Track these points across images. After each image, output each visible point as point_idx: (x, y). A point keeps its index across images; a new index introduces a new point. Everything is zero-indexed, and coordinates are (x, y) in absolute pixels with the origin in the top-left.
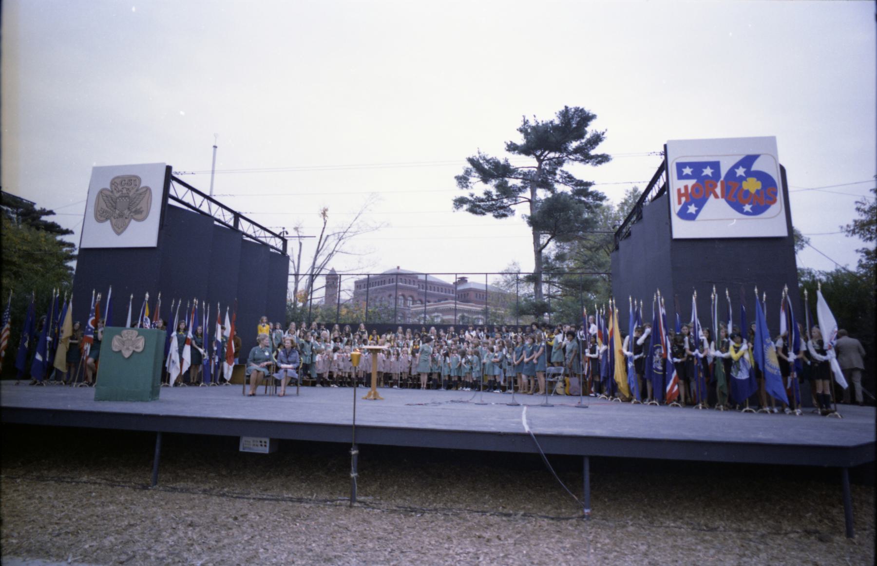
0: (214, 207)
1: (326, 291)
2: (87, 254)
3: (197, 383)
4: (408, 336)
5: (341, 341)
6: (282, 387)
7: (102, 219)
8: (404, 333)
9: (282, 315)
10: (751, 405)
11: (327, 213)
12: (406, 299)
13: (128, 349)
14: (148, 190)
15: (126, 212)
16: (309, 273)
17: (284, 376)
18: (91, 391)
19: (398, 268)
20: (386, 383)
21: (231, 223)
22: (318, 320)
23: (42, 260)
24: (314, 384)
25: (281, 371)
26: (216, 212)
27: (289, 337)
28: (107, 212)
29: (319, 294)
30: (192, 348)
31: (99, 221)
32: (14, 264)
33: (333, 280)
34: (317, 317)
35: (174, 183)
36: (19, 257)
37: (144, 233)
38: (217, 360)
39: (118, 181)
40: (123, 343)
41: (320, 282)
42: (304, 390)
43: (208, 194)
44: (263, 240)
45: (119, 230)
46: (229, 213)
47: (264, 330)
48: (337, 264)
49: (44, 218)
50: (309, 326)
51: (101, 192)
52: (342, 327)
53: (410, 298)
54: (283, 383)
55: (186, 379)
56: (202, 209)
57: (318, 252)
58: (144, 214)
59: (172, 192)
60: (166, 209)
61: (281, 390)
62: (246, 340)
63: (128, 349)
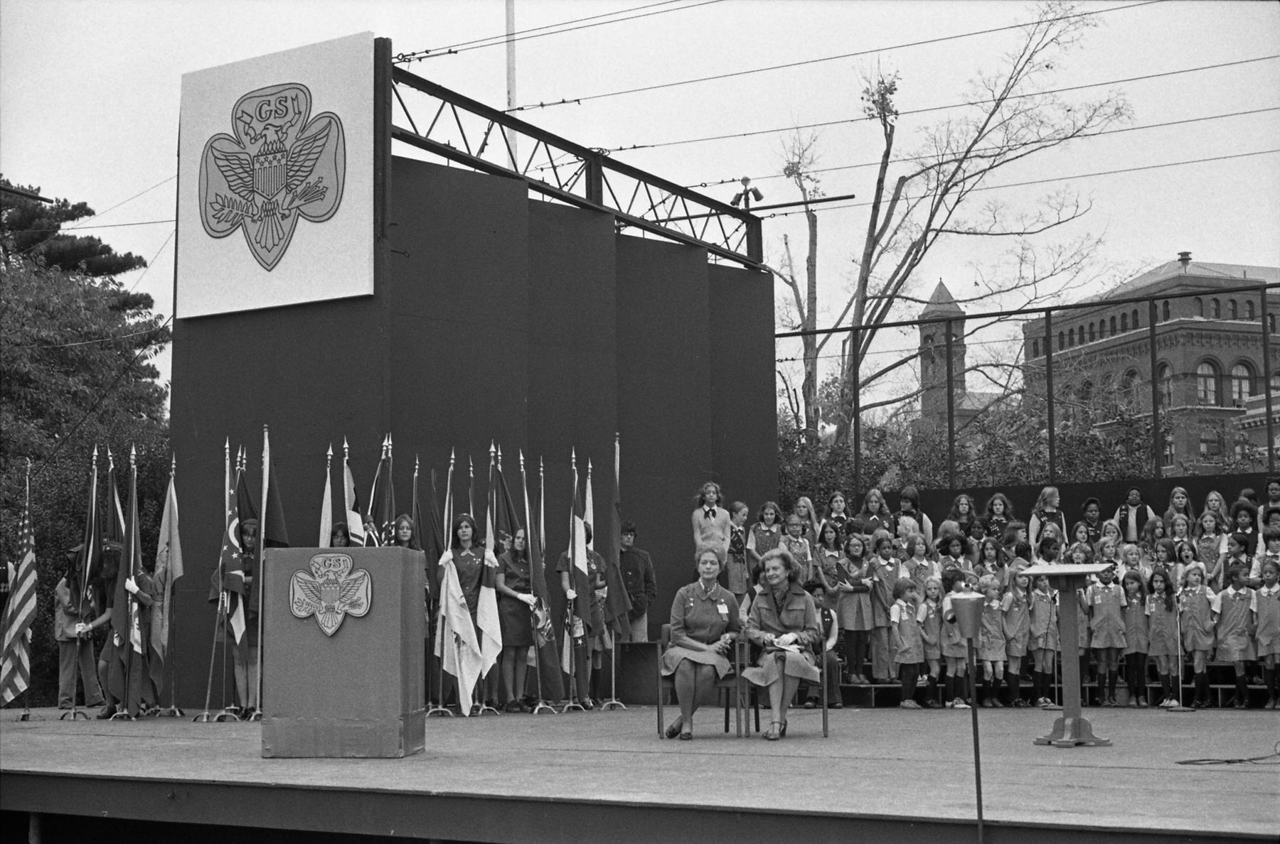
0: (525, 143)
1: (924, 370)
2: (195, 335)
3: (527, 705)
4: (1208, 521)
5: (966, 551)
6: (776, 713)
7: (224, 226)
8: (1196, 506)
9: (768, 471)
10: (546, 699)
11: (895, 100)
12: (1222, 378)
13: (330, 609)
14: (332, 120)
15: (282, 198)
16: (848, 322)
17: (775, 676)
18: (252, 732)
19: (1185, 258)
20: (1136, 691)
21: (580, 190)
22: (889, 479)
23: (82, 364)
24: (888, 699)
25: (768, 659)
26: (531, 160)
27: (788, 549)
28: (232, 203)
29: (893, 384)
30: (501, 596)
31: (217, 235)
32: (25, 380)
33: (943, 331)
34: (882, 470)
35: (402, 88)
36: (33, 359)
37: (333, 260)
38: (579, 632)
39: (250, 107)
40: (316, 592)
41: (894, 344)
42: (845, 719)
43: (500, 106)
44: (683, 228)
45: (269, 255)
46: (571, 157)
47: (714, 530)
48: (950, 271)
49: (68, 228)
50: (858, 502)
51: (210, 146)
52: (981, 496)
53: (1241, 371)
54: (775, 696)
55: (493, 694)
56: (491, 156)
57: (873, 240)
58: (330, 196)
59: (399, 120)
60: (389, 173)
61: (770, 720)
62: (650, 574)
63: (330, 609)
